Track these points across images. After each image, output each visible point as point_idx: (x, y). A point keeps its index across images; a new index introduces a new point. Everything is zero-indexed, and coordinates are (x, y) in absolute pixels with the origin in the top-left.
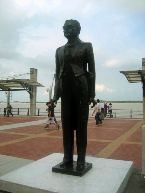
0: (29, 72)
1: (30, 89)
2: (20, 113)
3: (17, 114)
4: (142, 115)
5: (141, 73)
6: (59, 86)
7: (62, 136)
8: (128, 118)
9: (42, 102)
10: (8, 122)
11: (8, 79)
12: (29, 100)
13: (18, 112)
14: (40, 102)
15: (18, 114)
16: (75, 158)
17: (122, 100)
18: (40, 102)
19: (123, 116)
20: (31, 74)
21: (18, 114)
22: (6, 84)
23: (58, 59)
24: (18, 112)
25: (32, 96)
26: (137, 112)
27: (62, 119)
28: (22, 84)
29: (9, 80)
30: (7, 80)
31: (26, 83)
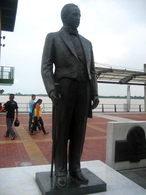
7: (87, 130)
11: (112, 68)
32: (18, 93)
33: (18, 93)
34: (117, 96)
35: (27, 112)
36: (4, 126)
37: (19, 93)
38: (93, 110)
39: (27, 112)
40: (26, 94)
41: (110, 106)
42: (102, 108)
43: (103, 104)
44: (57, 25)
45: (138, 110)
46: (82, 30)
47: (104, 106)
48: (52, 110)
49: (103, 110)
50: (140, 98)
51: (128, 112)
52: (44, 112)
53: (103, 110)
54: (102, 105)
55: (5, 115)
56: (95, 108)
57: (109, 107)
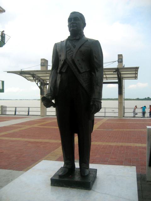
0: (117, 59)
1: (42, 84)
2: (17, 113)
3: (14, 114)
4: (118, 113)
5: (119, 70)
6: (56, 81)
7: (60, 139)
8: (13, 115)
9: (6, 99)
10: (23, 126)
11: (22, 70)
12: (116, 96)
13: (15, 111)
14: (3, 100)
15: (15, 114)
16: (77, 165)
17: (113, 98)
18: (3, 100)
19: (101, 114)
20: (118, 62)
21: (15, 114)
22: (38, 74)
23: (56, 47)
24: (15, 111)
25: (44, 92)
26: (35, 109)
27: (57, 120)
28: (34, 77)
29: (23, 71)
30: (21, 71)
31: (39, 77)
32: (147, 98)
33: (147, 98)
34: (144, 98)
35: (104, 117)
36: (133, 131)
37: (149, 98)
38: (96, 115)
39: (104, 117)
40: (127, 98)
41: (23, 109)
42: (14, 110)
43: (16, 107)
44: (64, 34)
45: (132, 115)
46: (89, 33)
47: (30, 109)
48: (55, 114)
49: (28, 113)
50: (127, 100)
51: (123, 117)
52: (105, 117)
53: (28, 113)
54: (28, 108)
55: (55, 118)
56: (98, 112)
57: (38, 109)
